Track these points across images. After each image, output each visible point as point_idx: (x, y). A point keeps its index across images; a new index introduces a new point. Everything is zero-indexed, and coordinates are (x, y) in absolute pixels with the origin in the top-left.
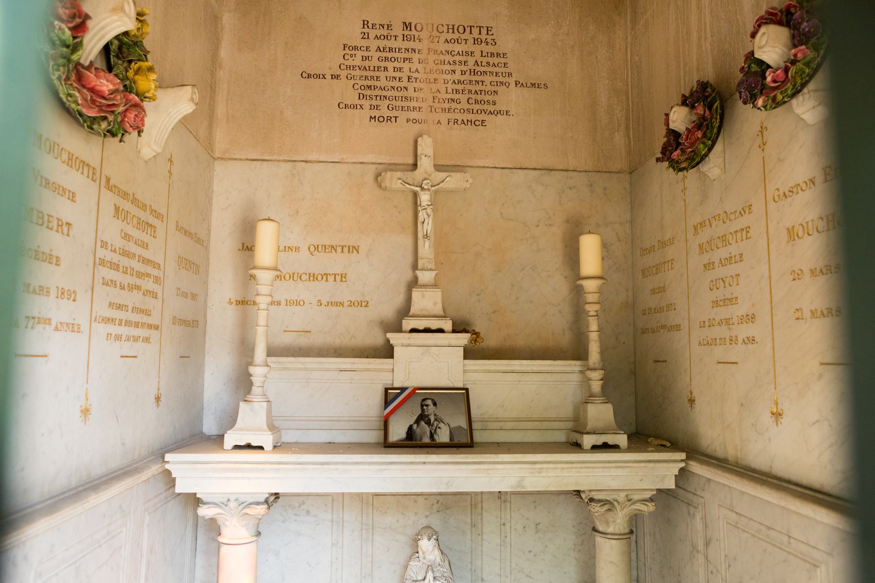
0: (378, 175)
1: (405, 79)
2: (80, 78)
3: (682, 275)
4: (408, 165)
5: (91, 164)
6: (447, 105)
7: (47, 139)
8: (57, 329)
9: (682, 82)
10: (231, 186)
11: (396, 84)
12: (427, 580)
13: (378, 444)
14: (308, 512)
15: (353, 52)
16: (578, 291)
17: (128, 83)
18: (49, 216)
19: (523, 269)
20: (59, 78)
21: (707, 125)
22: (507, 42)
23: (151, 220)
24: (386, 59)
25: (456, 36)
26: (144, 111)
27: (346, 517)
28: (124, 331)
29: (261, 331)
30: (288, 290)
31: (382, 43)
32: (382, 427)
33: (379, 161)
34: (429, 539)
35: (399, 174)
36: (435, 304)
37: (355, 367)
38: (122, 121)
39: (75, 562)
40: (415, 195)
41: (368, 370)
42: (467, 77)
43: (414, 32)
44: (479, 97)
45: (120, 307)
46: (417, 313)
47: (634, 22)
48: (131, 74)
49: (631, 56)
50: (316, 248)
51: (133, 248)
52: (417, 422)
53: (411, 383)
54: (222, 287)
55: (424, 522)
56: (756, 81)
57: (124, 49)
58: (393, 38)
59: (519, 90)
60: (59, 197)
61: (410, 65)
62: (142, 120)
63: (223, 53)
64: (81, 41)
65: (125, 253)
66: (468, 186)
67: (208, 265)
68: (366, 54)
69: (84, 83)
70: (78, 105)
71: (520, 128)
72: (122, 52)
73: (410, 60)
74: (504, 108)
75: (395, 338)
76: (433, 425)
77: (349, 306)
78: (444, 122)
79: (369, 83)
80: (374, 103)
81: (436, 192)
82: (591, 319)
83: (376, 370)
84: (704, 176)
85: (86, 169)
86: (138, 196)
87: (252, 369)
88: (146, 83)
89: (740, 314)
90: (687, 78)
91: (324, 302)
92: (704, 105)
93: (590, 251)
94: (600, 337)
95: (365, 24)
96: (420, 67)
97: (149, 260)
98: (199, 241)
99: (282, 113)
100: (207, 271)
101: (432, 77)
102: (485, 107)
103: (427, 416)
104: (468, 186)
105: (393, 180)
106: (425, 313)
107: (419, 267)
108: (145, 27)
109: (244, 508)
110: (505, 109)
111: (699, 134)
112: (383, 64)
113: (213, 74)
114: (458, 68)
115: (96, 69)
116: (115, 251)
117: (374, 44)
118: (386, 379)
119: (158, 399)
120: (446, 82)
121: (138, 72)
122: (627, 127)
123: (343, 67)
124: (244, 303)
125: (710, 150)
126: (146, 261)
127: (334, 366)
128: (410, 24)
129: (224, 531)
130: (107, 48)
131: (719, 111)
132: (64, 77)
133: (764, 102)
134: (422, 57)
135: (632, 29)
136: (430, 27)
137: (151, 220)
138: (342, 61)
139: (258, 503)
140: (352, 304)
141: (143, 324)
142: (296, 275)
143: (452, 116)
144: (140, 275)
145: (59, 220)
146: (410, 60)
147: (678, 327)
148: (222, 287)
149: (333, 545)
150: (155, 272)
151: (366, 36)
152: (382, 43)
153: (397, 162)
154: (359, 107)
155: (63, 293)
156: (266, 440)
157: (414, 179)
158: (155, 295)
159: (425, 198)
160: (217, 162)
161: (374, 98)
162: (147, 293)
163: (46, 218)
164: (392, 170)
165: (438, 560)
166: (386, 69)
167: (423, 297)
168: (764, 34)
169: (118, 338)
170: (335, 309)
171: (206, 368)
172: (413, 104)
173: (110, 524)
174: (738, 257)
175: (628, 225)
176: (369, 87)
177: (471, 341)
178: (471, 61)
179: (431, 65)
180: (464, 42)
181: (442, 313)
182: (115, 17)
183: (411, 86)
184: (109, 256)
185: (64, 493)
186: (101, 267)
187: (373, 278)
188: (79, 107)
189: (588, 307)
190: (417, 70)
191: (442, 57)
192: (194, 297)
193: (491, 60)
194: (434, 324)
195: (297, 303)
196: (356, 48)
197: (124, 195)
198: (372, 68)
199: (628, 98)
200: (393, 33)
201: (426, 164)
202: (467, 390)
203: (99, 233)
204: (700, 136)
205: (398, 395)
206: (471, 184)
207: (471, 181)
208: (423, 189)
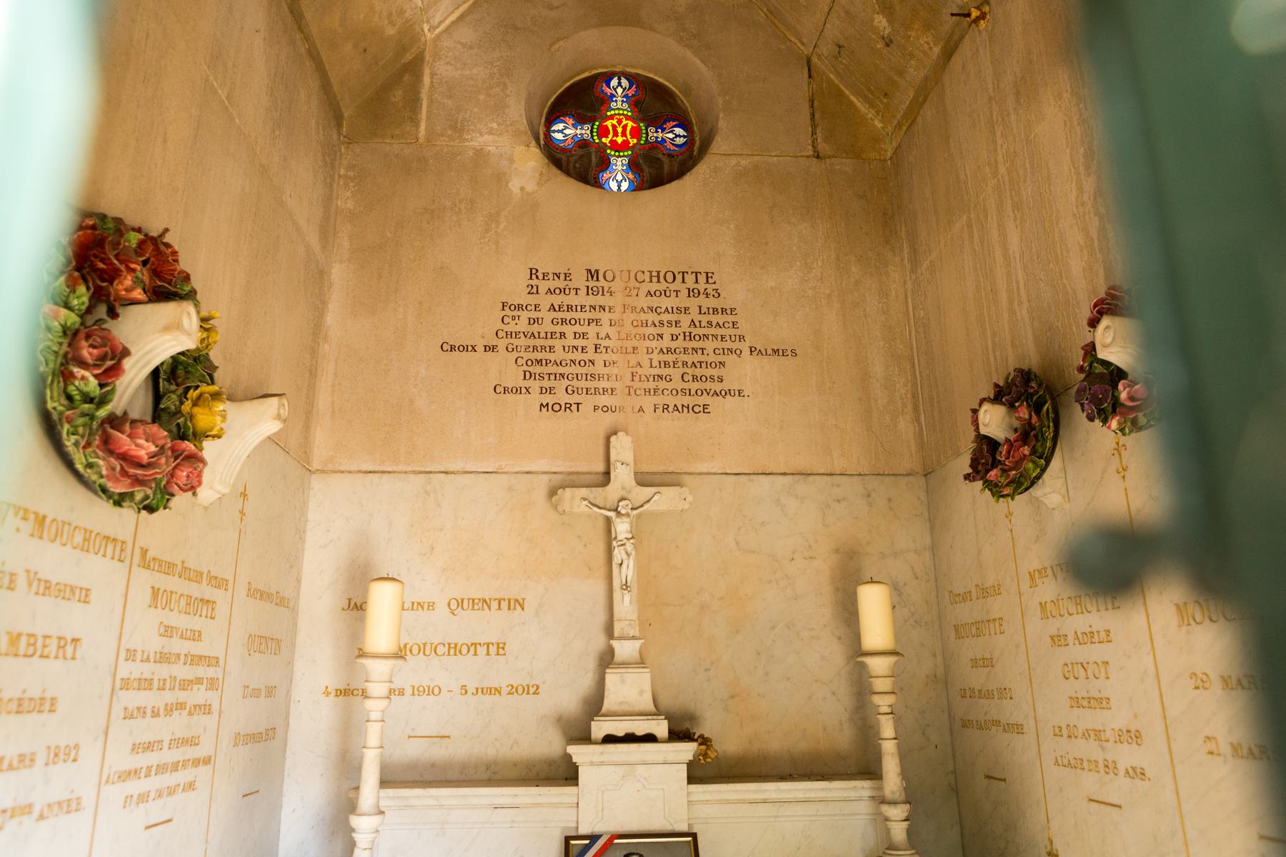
0: (552, 493)
1: (591, 349)
2: (106, 442)
3: (1018, 646)
5: (120, 537)
6: (652, 385)
9: (992, 359)
10: (334, 516)
11: (578, 356)
15: (516, 313)
16: (857, 652)
19: (773, 628)
20: (76, 444)
21: (1036, 436)
22: (735, 291)
24: (563, 321)
25: (663, 286)
29: (373, 735)
30: (415, 672)
31: (557, 300)
35: (583, 492)
36: (641, 693)
37: (518, 801)
40: (608, 521)
41: (537, 805)
42: (680, 343)
43: (602, 282)
44: (698, 372)
45: (149, 747)
46: (615, 708)
47: (915, 263)
48: (186, 407)
49: (914, 308)
50: (460, 603)
51: (178, 646)
54: (315, 668)
56: (1103, 389)
57: (180, 372)
58: (573, 292)
59: (756, 359)
60: (65, 602)
61: (597, 329)
62: (199, 476)
63: (330, 319)
64: (113, 390)
65: (164, 658)
67: (294, 637)
68: (534, 315)
69: (111, 447)
70: (102, 477)
71: (759, 415)
72: (180, 378)
73: (597, 321)
74: (735, 386)
75: (579, 753)
77: (509, 693)
78: (649, 408)
79: (539, 356)
80: (546, 384)
81: (639, 516)
82: (883, 719)
83: (551, 805)
84: (1037, 504)
86: (189, 564)
87: (355, 821)
89: (1116, 725)
90: (998, 353)
91: (471, 689)
92: (1029, 406)
93: (876, 625)
94: (899, 747)
95: (533, 273)
96: (612, 332)
97: (201, 657)
99: (412, 401)
100: (293, 645)
101: (629, 344)
102: (708, 385)
104: (687, 506)
105: (574, 500)
106: (626, 708)
107: (616, 634)
108: (213, 334)
110: (737, 388)
111: (1026, 450)
112: (559, 329)
113: (314, 352)
114: (667, 332)
115: (133, 422)
116: (148, 660)
117: (545, 301)
120: (649, 351)
121: (195, 404)
122: (916, 408)
123: (501, 334)
124: (349, 693)
125: (1043, 470)
126: (197, 660)
128: (597, 271)
130: (155, 373)
131: (1051, 415)
132: (83, 443)
133: (1119, 423)
134: (615, 317)
135: (913, 271)
136: (625, 275)
138: (500, 325)
140: (513, 690)
141: (185, 763)
143: (660, 400)
144: (186, 685)
146: (597, 321)
147: (1018, 729)
148: (315, 668)
151: (534, 290)
152: (557, 300)
153: (580, 470)
154: (524, 390)
155: (56, 755)
157: (605, 498)
158: (206, 709)
159: (622, 528)
160: (314, 476)
161: (546, 377)
163: (39, 644)
166: (563, 335)
167: (623, 682)
168: (1107, 327)
170: (487, 699)
171: (285, 800)
172: (602, 384)
174: (1103, 634)
175: (928, 555)
176: (539, 362)
177: (696, 756)
178: (685, 320)
179: (628, 328)
180: (674, 294)
181: (651, 708)
183: (599, 359)
187: (546, 660)
188: (103, 481)
189: (877, 699)
190: (608, 336)
191: (643, 317)
193: (715, 319)
194: (640, 728)
195: (430, 691)
196: (519, 307)
197: (167, 568)
198: (543, 335)
199: (913, 366)
200: (572, 285)
201: (622, 476)
202: (694, 836)
203: (125, 638)
204: (1027, 453)
205: (586, 848)
207: (690, 498)
208: (619, 514)
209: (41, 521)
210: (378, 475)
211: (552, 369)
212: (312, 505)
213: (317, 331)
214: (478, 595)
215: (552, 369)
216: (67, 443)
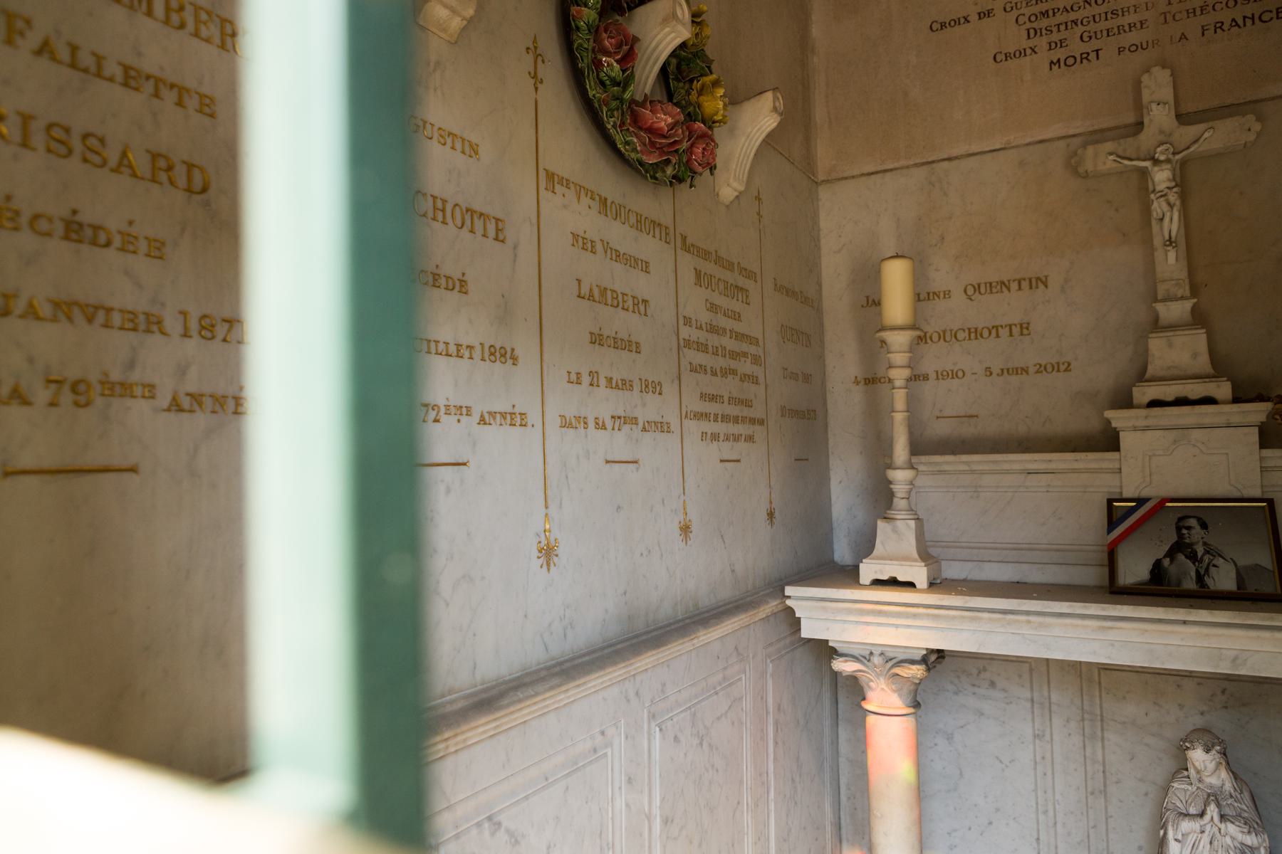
2: (636, 119)
4: (1126, 126)
5: (663, 221)
7: (456, 205)
8: (644, 430)
12: (1207, 818)
13: (1101, 587)
14: (993, 684)
17: (691, 109)
18: (623, 294)
20: (614, 126)
23: (742, 281)
26: (713, 141)
27: (1054, 697)
28: (721, 428)
32: (1106, 562)
33: (1072, 132)
34: (1207, 751)
35: (1109, 146)
36: (1195, 356)
37: (1053, 466)
38: (689, 160)
39: (690, 708)
40: (1144, 173)
41: (1074, 471)
45: (713, 398)
48: (693, 97)
50: (977, 288)
52: (1171, 554)
53: (1156, 490)
55: (1198, 721)
62: (712, 153)
63: (815, 31)
65: (713, 329)
66: (1252, 137)
67: (822, 333)
72: (684, 68)
75: (1118, 418)
76: (1201, 561)
77: (1037, 372)
80: (1055, 37)
81: (1184, 163)
85: (479, 224)
88: (714, 104)
91: (996, 370)
98: (806, 301)
100: (822, 341)
103: (1190, 545)
105: (1102, 159)
106: (1176, 372)
109: (893, 666)
116: (701, 328)
118: (1106, 485)
119: (771, 515)
121: (700, 93)
126: (740, 337)
127: (1016, 467)
129: (870, 694)
130: (664, 70)
137: (742, 281)
139: (913, 662)
140: (1041, 369)
141: (744, 419)
142: (948, 334)
143: (1210, 19)
144: (735, 355)
145: (634, 297)
149: (1036, 736)
150: (752, 350)
153: (1104, 126)
154: (1029, 51)
156: (919, 574)
158: (755, 380)
161: (1055, 29)
162: (746, 378)
164: (1097, 142)
165: (1228, 786)
167: (1170, 345)
169: (715, 437)
170: (1014, 380)
171: (832, 474)
173: (725, 668)
176: (1045, 14)
177: (1271, 415)
181: (1208, 369)
182: (667, 29)
184: (695, 335)
185: (670, 624)
186: (686, 350)
187: (1075, 322)
192: (807, 378)
194: (1195, 390)
195: (954, 375)
197: (705, 255)
201: (1160, 117)
202: (1271, 502)
205: (1131, 511)
206: (1259, 134)
207: (1257, 127)
209: (604, 202)
210: (879, 176)
211: (1061, 18)
212: (822, 215)
213: (804, 45)
214: (994, 278)
215: (1061, 18)
216: (609, 127)
